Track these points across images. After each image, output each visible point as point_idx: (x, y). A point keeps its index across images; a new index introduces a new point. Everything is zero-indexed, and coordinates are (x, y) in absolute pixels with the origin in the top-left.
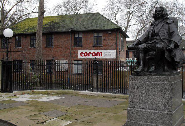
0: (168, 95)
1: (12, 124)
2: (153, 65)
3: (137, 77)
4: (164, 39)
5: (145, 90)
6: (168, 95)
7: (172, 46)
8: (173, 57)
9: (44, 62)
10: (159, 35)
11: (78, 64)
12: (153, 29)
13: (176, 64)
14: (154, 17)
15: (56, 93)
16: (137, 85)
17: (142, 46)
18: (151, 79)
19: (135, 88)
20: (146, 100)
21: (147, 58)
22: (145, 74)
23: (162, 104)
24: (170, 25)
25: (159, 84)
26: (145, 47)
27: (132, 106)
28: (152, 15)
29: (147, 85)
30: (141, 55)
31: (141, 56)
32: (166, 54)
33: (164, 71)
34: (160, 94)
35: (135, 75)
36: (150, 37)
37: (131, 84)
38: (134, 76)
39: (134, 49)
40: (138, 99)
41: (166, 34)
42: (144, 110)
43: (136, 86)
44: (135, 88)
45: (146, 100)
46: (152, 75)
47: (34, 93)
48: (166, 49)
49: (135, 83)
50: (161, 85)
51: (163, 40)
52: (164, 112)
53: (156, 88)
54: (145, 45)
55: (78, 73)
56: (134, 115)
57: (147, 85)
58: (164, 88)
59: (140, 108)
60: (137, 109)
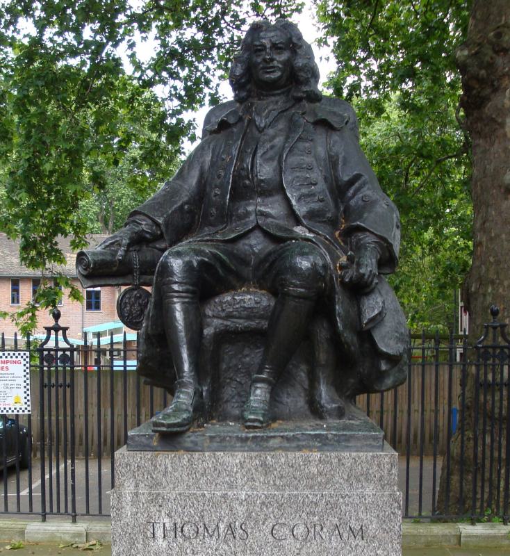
1: (198, 179)
2: (263, 381)
3: (166, 459)
5: (226, 542)
7: (369, 265)
10: (282, 190)
15: (15, 293)
16: (169, 515)
17: (469, 123)
18: (266, 469)
19: (159, 533)
21: (208, 331)
22: (223, 440)
25: (322, 504)
29: (241, 510)
31: (179, 315)
33: (316, 411)
35: (153, 449)
38: (149, 455)
43: (166, 520)
44: (159, 533)
46: (272, 443)
50: (332, 506)
53: (300, 530)
55: (99, 457)
57: (241, 510)
58: (353, 524)
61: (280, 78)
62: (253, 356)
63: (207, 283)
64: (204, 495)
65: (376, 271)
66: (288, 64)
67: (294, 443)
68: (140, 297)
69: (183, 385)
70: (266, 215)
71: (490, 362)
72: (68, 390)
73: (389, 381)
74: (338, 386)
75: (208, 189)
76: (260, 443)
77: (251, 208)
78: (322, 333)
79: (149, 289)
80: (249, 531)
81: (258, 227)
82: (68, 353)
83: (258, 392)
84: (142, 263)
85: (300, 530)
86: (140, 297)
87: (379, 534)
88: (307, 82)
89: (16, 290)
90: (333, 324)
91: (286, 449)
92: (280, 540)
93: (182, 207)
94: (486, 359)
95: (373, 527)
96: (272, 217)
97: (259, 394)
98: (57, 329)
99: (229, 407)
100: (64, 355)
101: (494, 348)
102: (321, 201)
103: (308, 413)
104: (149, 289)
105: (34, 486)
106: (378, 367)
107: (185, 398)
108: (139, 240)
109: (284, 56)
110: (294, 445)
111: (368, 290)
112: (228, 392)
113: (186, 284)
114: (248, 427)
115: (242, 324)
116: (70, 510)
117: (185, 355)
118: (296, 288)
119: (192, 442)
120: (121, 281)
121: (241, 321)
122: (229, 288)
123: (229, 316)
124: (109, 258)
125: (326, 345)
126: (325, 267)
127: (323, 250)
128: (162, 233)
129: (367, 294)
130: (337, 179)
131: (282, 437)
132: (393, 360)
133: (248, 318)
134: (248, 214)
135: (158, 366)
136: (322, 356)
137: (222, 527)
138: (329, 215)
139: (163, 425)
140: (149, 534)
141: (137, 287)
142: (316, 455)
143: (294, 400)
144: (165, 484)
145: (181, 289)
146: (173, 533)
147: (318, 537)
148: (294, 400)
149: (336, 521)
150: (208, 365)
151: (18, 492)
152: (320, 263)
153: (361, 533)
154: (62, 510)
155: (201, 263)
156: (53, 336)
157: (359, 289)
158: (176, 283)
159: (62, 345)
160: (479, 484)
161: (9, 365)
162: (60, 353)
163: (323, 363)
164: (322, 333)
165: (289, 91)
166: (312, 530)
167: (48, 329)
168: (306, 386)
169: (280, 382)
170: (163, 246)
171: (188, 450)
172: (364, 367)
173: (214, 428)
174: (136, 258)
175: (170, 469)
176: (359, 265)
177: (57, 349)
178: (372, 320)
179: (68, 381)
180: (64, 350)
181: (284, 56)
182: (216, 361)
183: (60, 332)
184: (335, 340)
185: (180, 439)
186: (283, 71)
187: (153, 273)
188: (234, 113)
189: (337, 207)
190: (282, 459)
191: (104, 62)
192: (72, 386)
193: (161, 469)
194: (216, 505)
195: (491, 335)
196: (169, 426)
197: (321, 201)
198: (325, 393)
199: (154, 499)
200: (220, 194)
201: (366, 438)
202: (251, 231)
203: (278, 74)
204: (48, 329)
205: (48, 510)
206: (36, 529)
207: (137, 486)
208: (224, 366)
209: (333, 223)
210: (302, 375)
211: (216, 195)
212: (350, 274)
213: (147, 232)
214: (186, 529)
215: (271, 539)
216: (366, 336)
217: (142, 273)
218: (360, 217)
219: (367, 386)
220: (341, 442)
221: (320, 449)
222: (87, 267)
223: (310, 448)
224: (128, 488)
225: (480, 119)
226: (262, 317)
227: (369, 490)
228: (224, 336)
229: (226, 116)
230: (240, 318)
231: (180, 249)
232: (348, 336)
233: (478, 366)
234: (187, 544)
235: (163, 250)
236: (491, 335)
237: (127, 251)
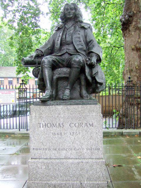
0: (97, 133)
2: (68, 89)
3: (43, 108)
4: (80, 49)
6: (97, 133)
7: (94, 60)
8: (94, 76)
9: (31, 87)
10: (72, 43)
11: (122, 85)
12: (63, 34)
13: (99, 86)
16: (44, 121)
18: (68, 110)
19: (41, 126)
21: (55, 77)
23: (87, 149)
24: (86, 31)
26: (53, 60)
27: (37, 156)
28: (68, 3)
29: (62, 120)
30: (47, 72)
32: (87, 70)
35: (40, 105)
36: (57, 46)
38: (39, 106)
39: (124, 3)
41: (83, 42)
43: (43, 123)
44: (41, 126)
48: (87, 64)
51: (78, 51)
52: (90, 160)
53: (77, 125)
54: (54, 57)
57: (62, 120)
60: (46, 161)
61: (72, 17)
62: (65, 83)
63: (54, 66)
68: (38, 70)
69: (47, 89)
70: (69, 49)
74: (87, 91)
77: (65, 48)
78: (83, 78)
79: (40, 68)
80: (64, 125)
81: (67, 52)
82: (25, 90)
85: (77, 125)
86: (38, 70)
87: (97, 125)
90: (85, 74)
92: (72, 127)
95: (95, 124)
96: (70, 50)
97: (67, 92)
100: (25, 90)
104: (40, 68)
109: (74, 11)
111: (94, 67)
116: (26, 128)
120: (33, 66)
121: (63, 75)
123: (60, 74)
125: (84, 80)
129: (94, 68)
130: (86, 41)
133: (64, 74)
134: (64, 49)
136: (83, 83)
137: (57, 124)
140: (39, 126)
144: (43, 114)
146: (45, 126)
147: (81, 126)
148: (76, 94)
149: (86, 122)
153: (92, 125)
154: (24, 128)
156: (22, 86)
157: (91, 66)
158: (46, 65)
159: (24, 87)
161: (11, 93)
162: (24, 90)
163: (83, 85)
164: (83, 78)
165: (75, 20)
166: (80, 125)
169: (72, 89)
172: (94, 86)
176: (91, 60)
177: (23, 89)
178: (95, 74)
180: (24, 89)
181: (74, 11)
182: (57, 85)
183: (23, 85)
184: (86, 78)
185: (46, 103)
186: (73, 15)
189: (86, 48)
191: (133, 166)
198: (84, 92)
199: (40, 117)
202: (64, 54)
203: (72, 16)
204: (21, 84)
205: (21, 128)
207: (36, 114)
210: (78, 88)
212: (89, 63)
213: (40, 54)
214: (48, 125)
215: (69, 127)
217: (38, 64)
222: (24, 62)
226: (68, 74)
227: (94, 114)
228: (59, 79)
232: (89, 78)
234: (48, 129)
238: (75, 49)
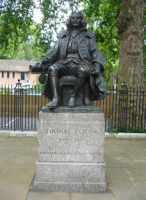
2: (73, 97)
3: (51, 114)
4: (85, 58)
6: (99, 140)
7: (97, 70)
8: (97, 85)
10: (78, 52)
14: (68, 26)
18: (74, 117)
20: (66, 150)
21: (61, 85)
22: (64, 110)
23: (90, 154)
29: (68, 126)
33: (84, 104)
34: (88, 139)
37: (42, 126)
40: (53, 148)
42: (63, 164)
43: (51, 129)
45: (66, 150)
47: (144, 61)
49: (48, 124)
50: (89, 126)
56: (47, 173)
57: (68, 126)
58: (94, 130)
59: (56, 162)
62: (70, 91)
63: (61, 73)
64: (59, 123)
65: (99, 72)
66: (80, 22)
67: (80, 111)
71: (123, 94)
72: (21, 99)
73: (101, 98)
75: (60, 51)
76: (72, 111)
83: (72, 99)
84: (45, 68)
88: (84, 26)
89: (3, 74)
91: (79, 113)
93: (54, 55)
94: (122, 94)
95: (98, 131)
97: (72, 100)
98: (19, 84)
99: (65, 103)
101: (124, 91)
102: (87, 55)
103: (83, 104)
105: (9, 123)
106: (99, 94)
107: (55, 100)
108: (44, 63)
109: (79, 20)
110: (80, 111)
112: (64, 99)
113: (56, 74)
114: (69, 107)
115: (68, 83)
116: (21, 129)
117: (55, 90)
118: (81, 75)
119: (57, 110)
122: (67, 75)
123: (65, 82)
124: (37, 67)
126: (88, 71)
127: (88, 67)
128: (49, 62)
129: (97, 77)
131: (78, 110)
132: (103, 93)
133: (70, 82)
135: (48, 93)
137: (63, 130)
138: (89, 58)
139: (51, 106)
141: (43, 74)
142: (85, 114)
143: (80, 101)
145: (54, 75)
150: (60, 94)
151: (5, 125)
152: (87, 70)
155: (59, 69)
157: (96, 76)
160: (119, 123)
164: (87, 86)
167: (17, 84)
168: (82, 98)
169: (76, 97)
170: (50, 64)
171: (56, 112)
173: (61, 108)
174: (43, 67)
175: (52, 117)
179: (21, 97)
181: (79, 20)
182: (62, 92)
184: (90, 88)
185: (54, 110)
187: (47, 71)
188: (67, 33)
190: (77, 115)
192: (22, 98)
193: (50, 117)
194: (62, 125)
195: (123, 88)
196: (52, 107)
197: (87, 55)
198: (87, 101)
200: (63, 53)
201: (97, 110)
204: (17, 84)
206: (13, 133)
207: (44, 120)
208: (63, 93)
209: (89, 60)
211: (62, 53)
214: (55, 130)
215: (75, 133)
216: (96, 87)
218: (96, 59)
219: (96, 99)
220: (91, 111)
221: (86, 113)
223: (85, 112)
224: (42, 121)
225: (121, 36)
228: (64, 86)
229: (65, 34)
230: (68, 82)
231: (55, 65)
232: (93, 87)
233: (120, 95)
235: (50, 66)
236: (123, 88)
237: (41, 65)
238: (80, 58)
